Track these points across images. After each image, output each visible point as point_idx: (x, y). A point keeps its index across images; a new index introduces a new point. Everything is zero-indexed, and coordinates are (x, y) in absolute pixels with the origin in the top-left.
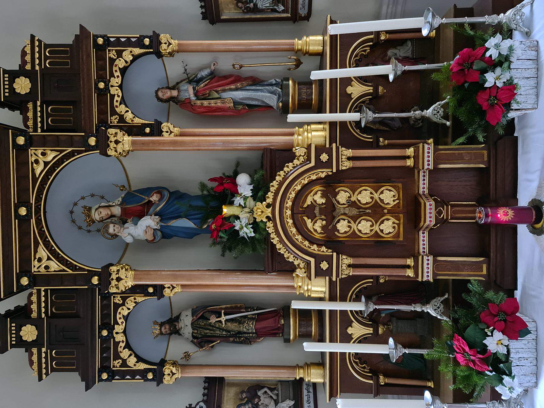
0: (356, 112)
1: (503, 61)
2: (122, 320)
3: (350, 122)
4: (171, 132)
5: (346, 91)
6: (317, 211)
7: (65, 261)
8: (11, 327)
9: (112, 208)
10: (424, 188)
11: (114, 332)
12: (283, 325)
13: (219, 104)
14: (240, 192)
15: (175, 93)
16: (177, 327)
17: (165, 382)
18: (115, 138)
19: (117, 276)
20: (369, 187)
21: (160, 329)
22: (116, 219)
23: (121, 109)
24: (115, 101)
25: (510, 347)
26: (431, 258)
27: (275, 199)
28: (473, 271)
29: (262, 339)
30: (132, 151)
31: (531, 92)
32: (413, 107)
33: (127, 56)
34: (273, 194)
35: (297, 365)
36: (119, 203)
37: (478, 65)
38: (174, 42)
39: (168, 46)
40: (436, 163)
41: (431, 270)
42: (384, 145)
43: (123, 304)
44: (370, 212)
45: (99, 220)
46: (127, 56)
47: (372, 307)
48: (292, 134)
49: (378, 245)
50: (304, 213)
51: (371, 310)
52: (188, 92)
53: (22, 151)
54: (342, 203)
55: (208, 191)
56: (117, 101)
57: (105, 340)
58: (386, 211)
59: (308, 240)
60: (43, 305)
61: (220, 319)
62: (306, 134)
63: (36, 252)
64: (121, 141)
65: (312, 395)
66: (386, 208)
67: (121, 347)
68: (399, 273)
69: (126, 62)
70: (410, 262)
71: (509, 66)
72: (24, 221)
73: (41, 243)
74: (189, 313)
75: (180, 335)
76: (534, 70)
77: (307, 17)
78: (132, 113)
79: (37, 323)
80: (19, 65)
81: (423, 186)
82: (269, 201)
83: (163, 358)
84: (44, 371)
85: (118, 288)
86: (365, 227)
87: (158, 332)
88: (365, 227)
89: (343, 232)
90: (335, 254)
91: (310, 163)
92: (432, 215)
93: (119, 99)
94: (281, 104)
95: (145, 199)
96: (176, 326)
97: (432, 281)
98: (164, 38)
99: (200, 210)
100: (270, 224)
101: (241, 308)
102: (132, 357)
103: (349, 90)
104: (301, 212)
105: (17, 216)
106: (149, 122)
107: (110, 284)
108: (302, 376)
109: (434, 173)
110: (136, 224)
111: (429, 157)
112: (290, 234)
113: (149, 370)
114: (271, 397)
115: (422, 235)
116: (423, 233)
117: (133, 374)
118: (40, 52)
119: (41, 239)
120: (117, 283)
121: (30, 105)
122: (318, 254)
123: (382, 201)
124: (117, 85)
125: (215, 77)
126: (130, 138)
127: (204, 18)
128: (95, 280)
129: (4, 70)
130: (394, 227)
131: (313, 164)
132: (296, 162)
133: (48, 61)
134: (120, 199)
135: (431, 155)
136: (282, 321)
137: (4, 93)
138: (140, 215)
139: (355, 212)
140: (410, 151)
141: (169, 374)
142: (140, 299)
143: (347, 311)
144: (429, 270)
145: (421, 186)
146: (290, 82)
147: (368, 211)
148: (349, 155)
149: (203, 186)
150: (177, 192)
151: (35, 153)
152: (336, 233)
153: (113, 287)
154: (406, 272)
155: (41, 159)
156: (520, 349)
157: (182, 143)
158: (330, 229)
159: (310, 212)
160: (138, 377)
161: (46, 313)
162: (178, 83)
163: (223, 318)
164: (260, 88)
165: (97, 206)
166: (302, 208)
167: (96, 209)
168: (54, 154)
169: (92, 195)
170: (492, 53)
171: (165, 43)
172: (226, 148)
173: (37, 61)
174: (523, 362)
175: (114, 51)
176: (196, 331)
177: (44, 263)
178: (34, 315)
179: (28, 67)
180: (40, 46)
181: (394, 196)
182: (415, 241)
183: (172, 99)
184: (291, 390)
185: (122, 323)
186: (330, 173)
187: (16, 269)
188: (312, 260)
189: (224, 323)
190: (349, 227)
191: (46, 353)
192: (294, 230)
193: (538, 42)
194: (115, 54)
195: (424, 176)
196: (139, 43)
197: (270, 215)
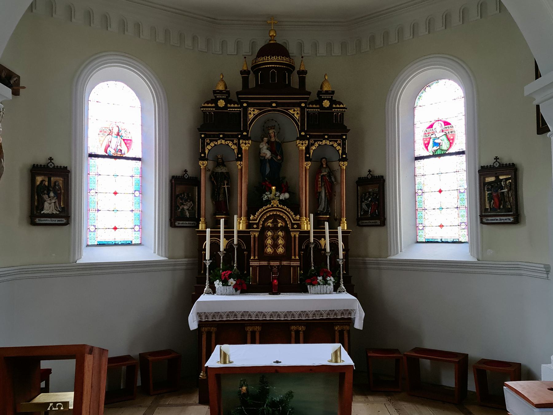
1: (326, 283)
15: (324, 166)
23: (317, 145)
33: (338, 148)
43: (233, 144)
46: (338, 148)
47: (235, 247)
48: (306, 217)
49: (263, 246)
53: (299, 105)
63: (257, 109)
70: (256, 257)
72: (270, 105)
79: (226, 107)
81: (285, 263)
86: (269, 242)
88: (269, 242)
98: (346, 163)
99: (271, 174)
103: (323, 239)
104: (275, 218)
109: (290, 266)
110: (267, 149)
127: (359, 178)
131: (293, 222)
139: (275, 237)
142: (236, 151)
151: (298, 110)
155: (295, 113)
156: (231, 289)
158: (269, 229)
159: (275, 222)
163: (226, 186)
168: (298, 118)
170: (328, 278)
174: (225, 290)
179: (334, 106)
183: (322, 164)
187: (249, 101)
196: (344, 153)
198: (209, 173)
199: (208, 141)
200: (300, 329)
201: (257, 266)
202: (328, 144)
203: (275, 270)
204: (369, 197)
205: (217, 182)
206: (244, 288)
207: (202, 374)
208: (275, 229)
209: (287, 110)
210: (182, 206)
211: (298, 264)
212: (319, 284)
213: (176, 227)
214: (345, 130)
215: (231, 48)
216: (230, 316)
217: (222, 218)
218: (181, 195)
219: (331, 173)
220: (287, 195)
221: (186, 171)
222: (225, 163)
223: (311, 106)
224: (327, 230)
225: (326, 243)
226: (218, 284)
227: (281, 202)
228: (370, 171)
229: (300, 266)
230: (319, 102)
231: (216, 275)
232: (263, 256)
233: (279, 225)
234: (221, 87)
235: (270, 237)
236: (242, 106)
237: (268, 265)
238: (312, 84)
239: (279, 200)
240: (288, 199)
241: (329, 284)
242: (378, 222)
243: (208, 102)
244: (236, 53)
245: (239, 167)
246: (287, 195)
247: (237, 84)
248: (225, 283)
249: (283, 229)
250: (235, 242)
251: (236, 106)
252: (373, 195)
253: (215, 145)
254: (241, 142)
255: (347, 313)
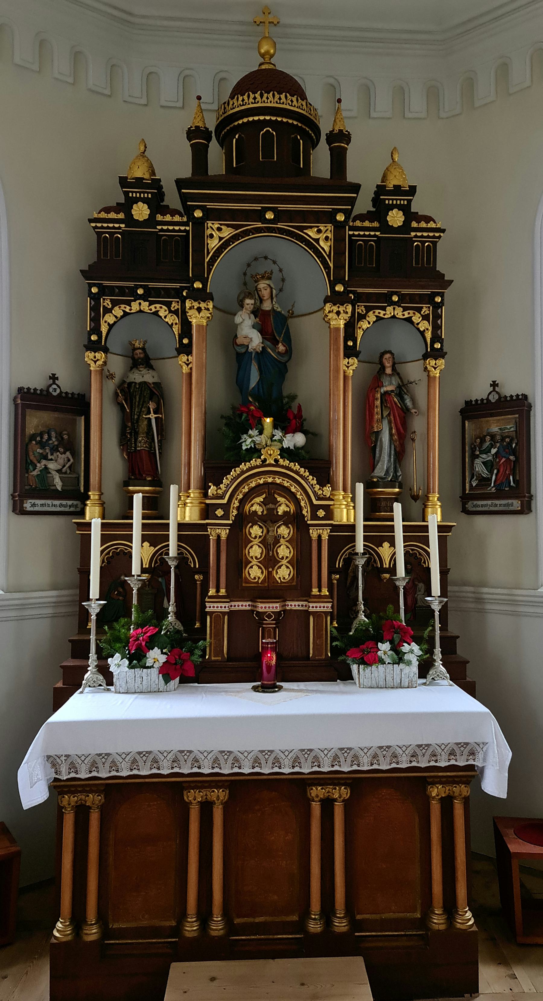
0: (364, 549)
1: (399, 658)
2: (154, 310)
3: (354, 546)
4: (348, 367)
5: (385, 541)
6: (271, 506)
7: (218, 255)
8: (148, 193)
9: (270, 301)
10: (291, 605)
11: (142, 301)
12: (145, 479)
13: (377, 417)
14: (287, 435)
15: (389, 371)
16: (141, 366)
17: (88, 353)
18: (342, 312)
19: (203, 308)
20: (293, 556)
21: (139, 348)
22: (258, 304)
23: (372, 317)
24: (380, 311)
25: (152, 669)
26: (227, 610)
27: (282, 467)
28: (215, 644)
29: (126, 457)
30: (329, 327)
31: (374, 682)
32: (369, 609)
33: (424, 325)
34: (287, 465)
35: (102, 494)
36: (275, 308)
37: (397, 637)
38: (437, 373)
39: (433, 367)
40: (314, 613)
41: (215, 609)
42: (332, 580)
43: (170, 311)
44: (267, 557)
45: (259, 287)
46: (424, 325)
47: (172, 564)
48: (345, 490)
49: (238, 563)
50: (269, 494)
51: (170, 563)
52: (389, 386)
53: (330, 217)
54: (278, 530)
55: (287, 403)
56: (379, 313)
57: (132, 292)
58: (271, 570)
59: (243, 498)
60: (171, 228)
61: (152, 412)
62: (345, 503)
63: (228, 226)
64: (340, 317)
65: (67, 509)
66: (273, 570)
67: (125, 308)
68: (212, 581)
69: (418, 324)
70: (223, 592)
71: (396, 664)
72: (259, 216)
73: (237, 232)
74: (156, 380)
75: (131, 369)
76: (392, 684)
77: (465, 511)
78: (368, 328)
79: (151, 221)
80: (417, 213)
81: (294, 605)
82: (281, 462)
83: (110, 351)
84: (99, 225)
85: (190, 308)
86: (255, 551)
87: (137, 345)
88: (255, 551)
89: (251, 531)
90: (231, 522)
91: (316, 500)
92: (267, 609)
93: (381, 315)
94: (375, 480)
95: (280, 337)
96: (143, 365)
97: (206, 610)
98: (441, 362)
99: (263, 390)
100: (259, 462)
101: (162, 436)
102: (114, 319)
103: (386, 545)
104: (271, 491)
105: (266, 210)
106: (358, 345)
107: (195, 301)
108: (92, 497)
109: (307, 613)
110: (254, 327)
111: (320, 607)
112: (249, 481)
113: (100, 336)
114: (64, 466)
115: (247, 604)
116: (249, 605)
117: (96, 320)
118: (428, 237)
119: (240, 232)
120: (196, 307)
121: (376, 224)
122: (230, 507)
123: (280, 567)
124: (396, 314)
125: (405, 413)
126: (342, 326)
127: (466, 402)
128: (198, 285)
129: (411, 200)
130: (255, 578)
131: (315, 502)
132: (318, 487)
133: (419, 244)
134: (279, 310)
135: (322, 609)
136: (150, 479)
137: (389, 200)
138: (262, 331)
139: (270, 541)
140: (325, 592)
141: (95, 357)
142: (176, 329)
143: (168, 541)
144: (215, 608)
145: (293, 603)
146: (397, 490)
147: (271, 553)
148: (323, 536)
149: (293, 398)
150: (430, 569)
151: (328, 230)
152: (250, 524)
153: (191, 304)
154: (213, 588)
155: (322, 236)
156: (152, 676)
157: (337, 378)
158: (254, 519)
159: (270, 501)
160: (93, 325)
161: (162, 230)
162: (398, 374)
163: (152, 416)
164: (392, 459)
165: (272, 286)
166: (274, 493)
167: (269, 285)
168: (327, 249)
169: (283, 280)
170: (406, 648)
171: (436, 364)
172: (331, 423)
173: (419, 234)
174: (138, 680)
175: (428, 312)
176: (138, 386)
177: (216, 234)
178: (159, 218)
179: (414, 224)
180: (434, 237)
181: (284, 578)
182: (242, 598)
183: (383, 368)
184: (71, 488)
185: (151, 310)
186: (306, 519)
187: (210, 205)
188: (225, 501)
189: (148, 416)
190: (256, 537)
191: (120, 228)
192: (253, 485)
193: (416, 687)
194: (426, 313)
195: (302, 606)
196: (436, 338)
197: (267, 462)
198: (111, 386)
199: (108, 303)
200: (336, 796)
201: (224, 613)
202: (400, 315)
203: (269, 622)
204: (492, 446)
205: (131, 408)
206: (188, 670)
207: (59, 925)
208: (270, 519)
209: (302, 229)
210: (44, 462)
211: (326, 607)
212: (383, 662)
213: (24, 513)
214: (443, 282)
215: (169, 91)
216: (141, 763)
217: (138, 492)
218: (41, 435)
219: (403, 389)
220: (299, 439)
221: (54, 378)
222: (152, 362)
223: (358, 223)
224: (398, 524)
225: (396, 553)
226: (117, 664)
227: (285, 453)
228: (494, 385)
229: (331, 614)
230: (380, 211)
231: (117, 639)
232: (237, 587)
233: (281, 510)
234: (140, 172)
235: (256, 541)
236: (191, 217)
237: (252, 611)
238: (364, 170)
239: (282, 450)
240: (303, 448)
241: (409, 663)
242: (516, 504)
243: (107, 210)
244: (180, 104)
245: (185, 369)
246: (299, 439)
247: (175, 163)
248: (139, 660)
249: (287, 519)
250: (173, 551)
251: (177, 218)
252: (503, 439)
253: (126, 314)
254: (188, 304)
255: (466, 752)
